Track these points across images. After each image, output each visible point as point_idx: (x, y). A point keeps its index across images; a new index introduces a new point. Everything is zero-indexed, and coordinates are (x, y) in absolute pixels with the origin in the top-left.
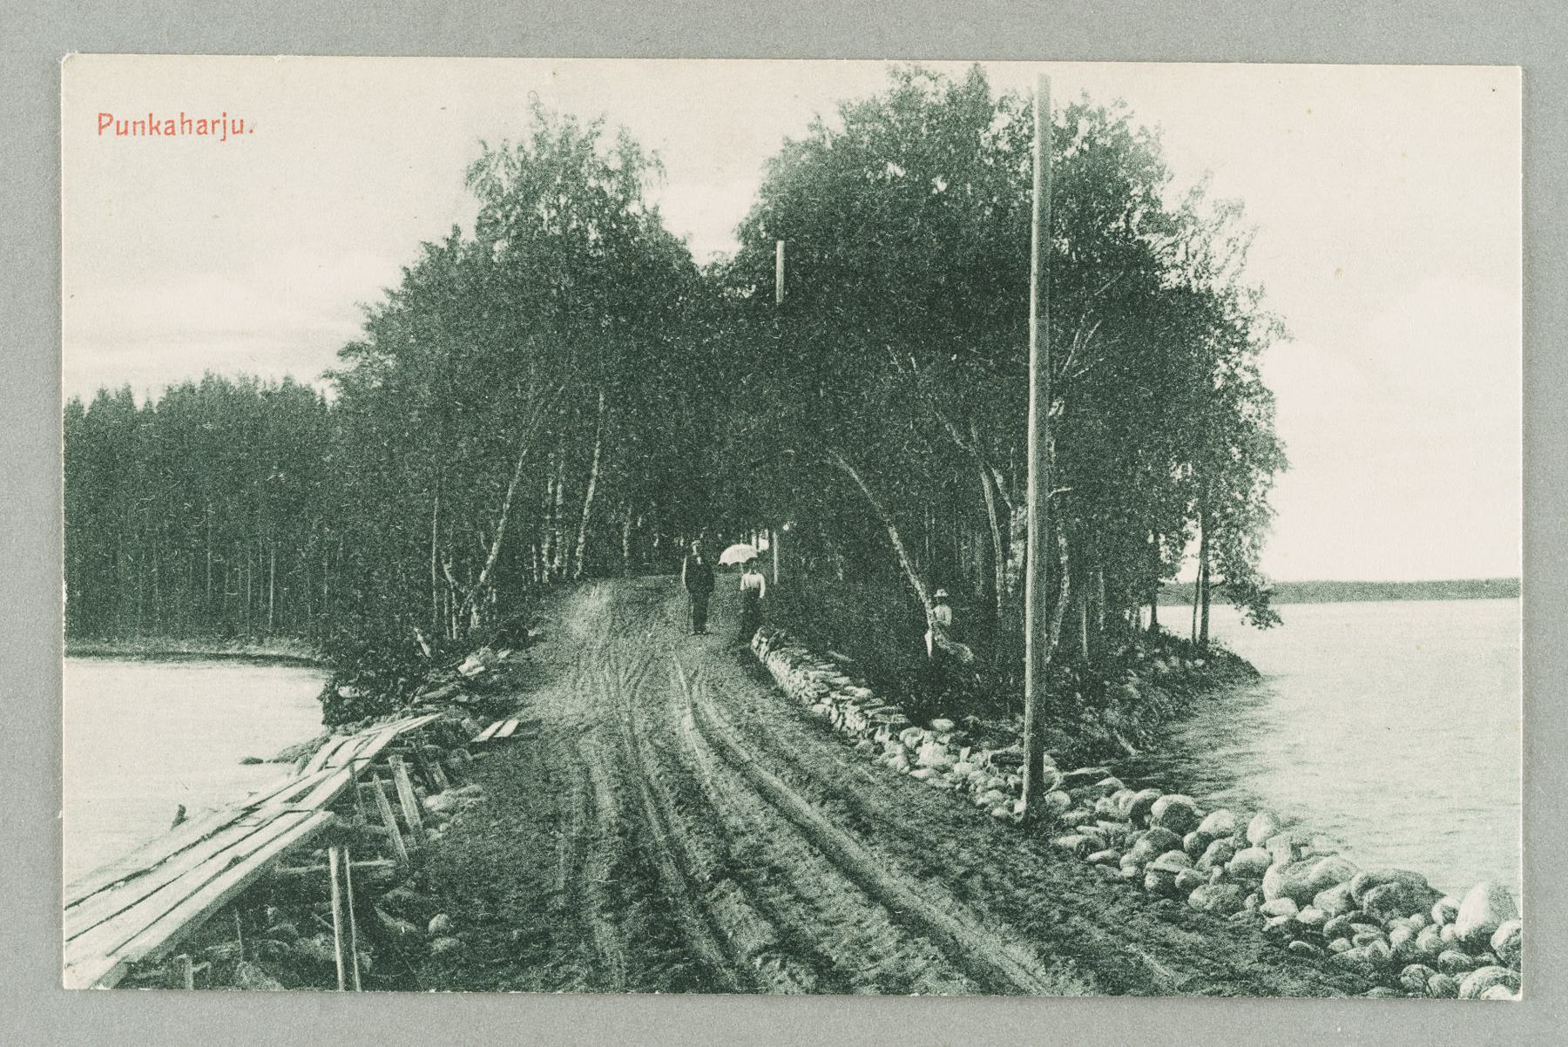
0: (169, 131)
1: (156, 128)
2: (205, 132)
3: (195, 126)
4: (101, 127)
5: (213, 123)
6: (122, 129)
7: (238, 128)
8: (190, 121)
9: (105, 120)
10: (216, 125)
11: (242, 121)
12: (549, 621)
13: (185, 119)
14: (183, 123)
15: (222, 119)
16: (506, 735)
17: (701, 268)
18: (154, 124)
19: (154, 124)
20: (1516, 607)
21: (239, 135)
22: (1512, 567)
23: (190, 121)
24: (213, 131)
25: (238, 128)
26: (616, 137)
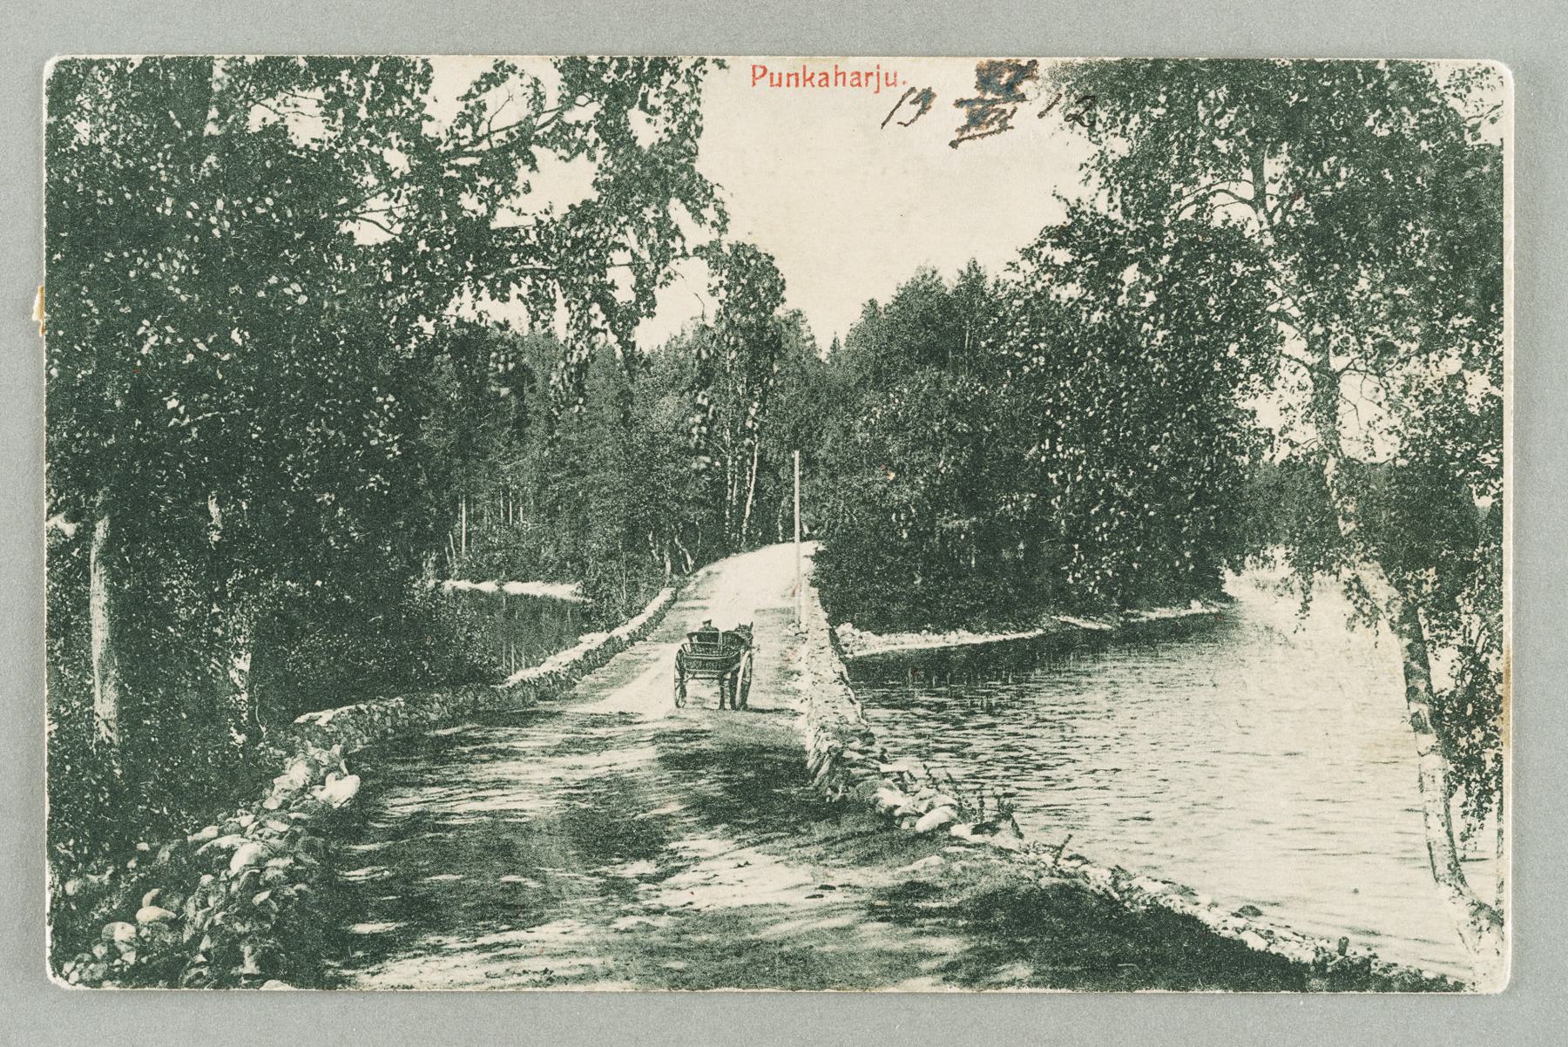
0: (824, 83)
3: (849, 78)
6: (776, 81)
13: (839, 71)
14: (837, 75)
25: (891, 80)
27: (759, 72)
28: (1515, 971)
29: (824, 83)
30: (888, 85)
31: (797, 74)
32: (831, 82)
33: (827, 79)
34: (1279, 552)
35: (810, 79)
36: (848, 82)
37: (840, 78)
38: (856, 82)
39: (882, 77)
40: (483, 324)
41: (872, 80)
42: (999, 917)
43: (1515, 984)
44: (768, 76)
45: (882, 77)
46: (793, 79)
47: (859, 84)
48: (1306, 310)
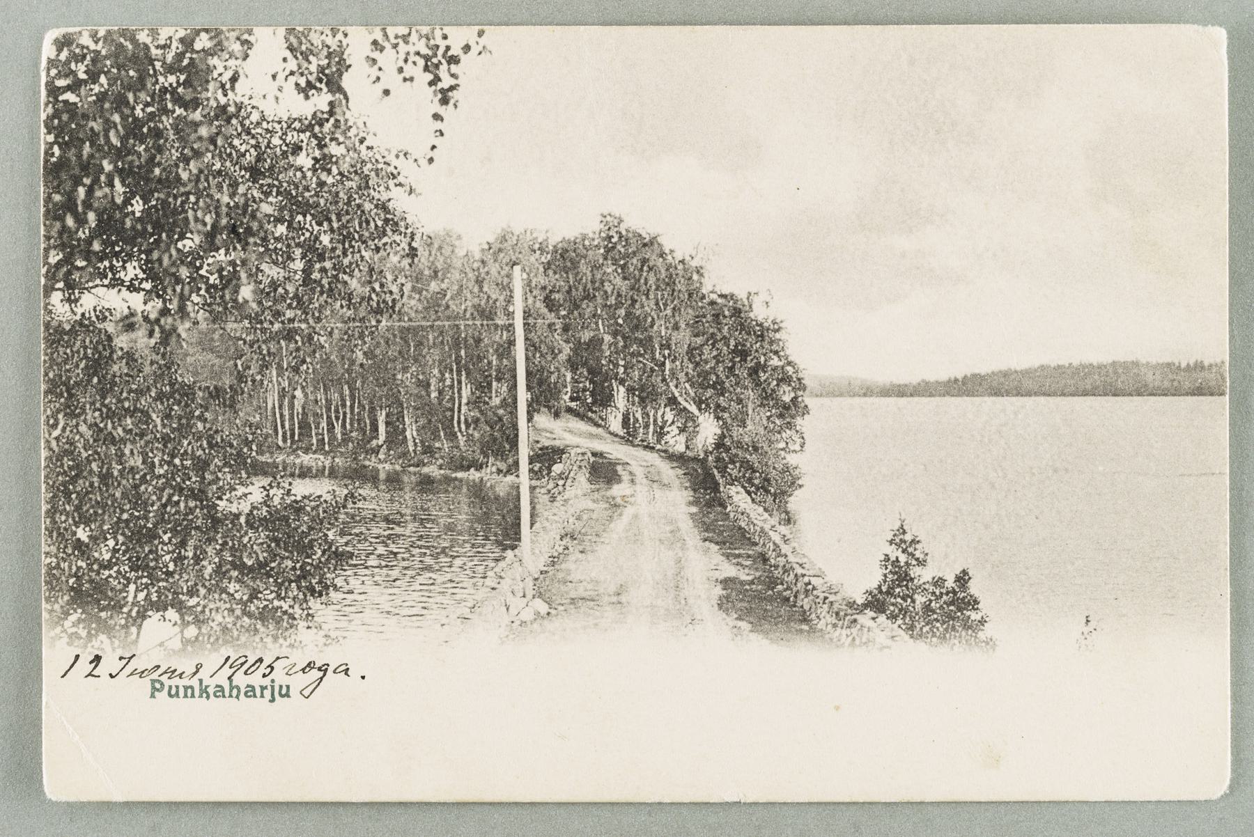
3: (243, 691)
11: (288, 687)
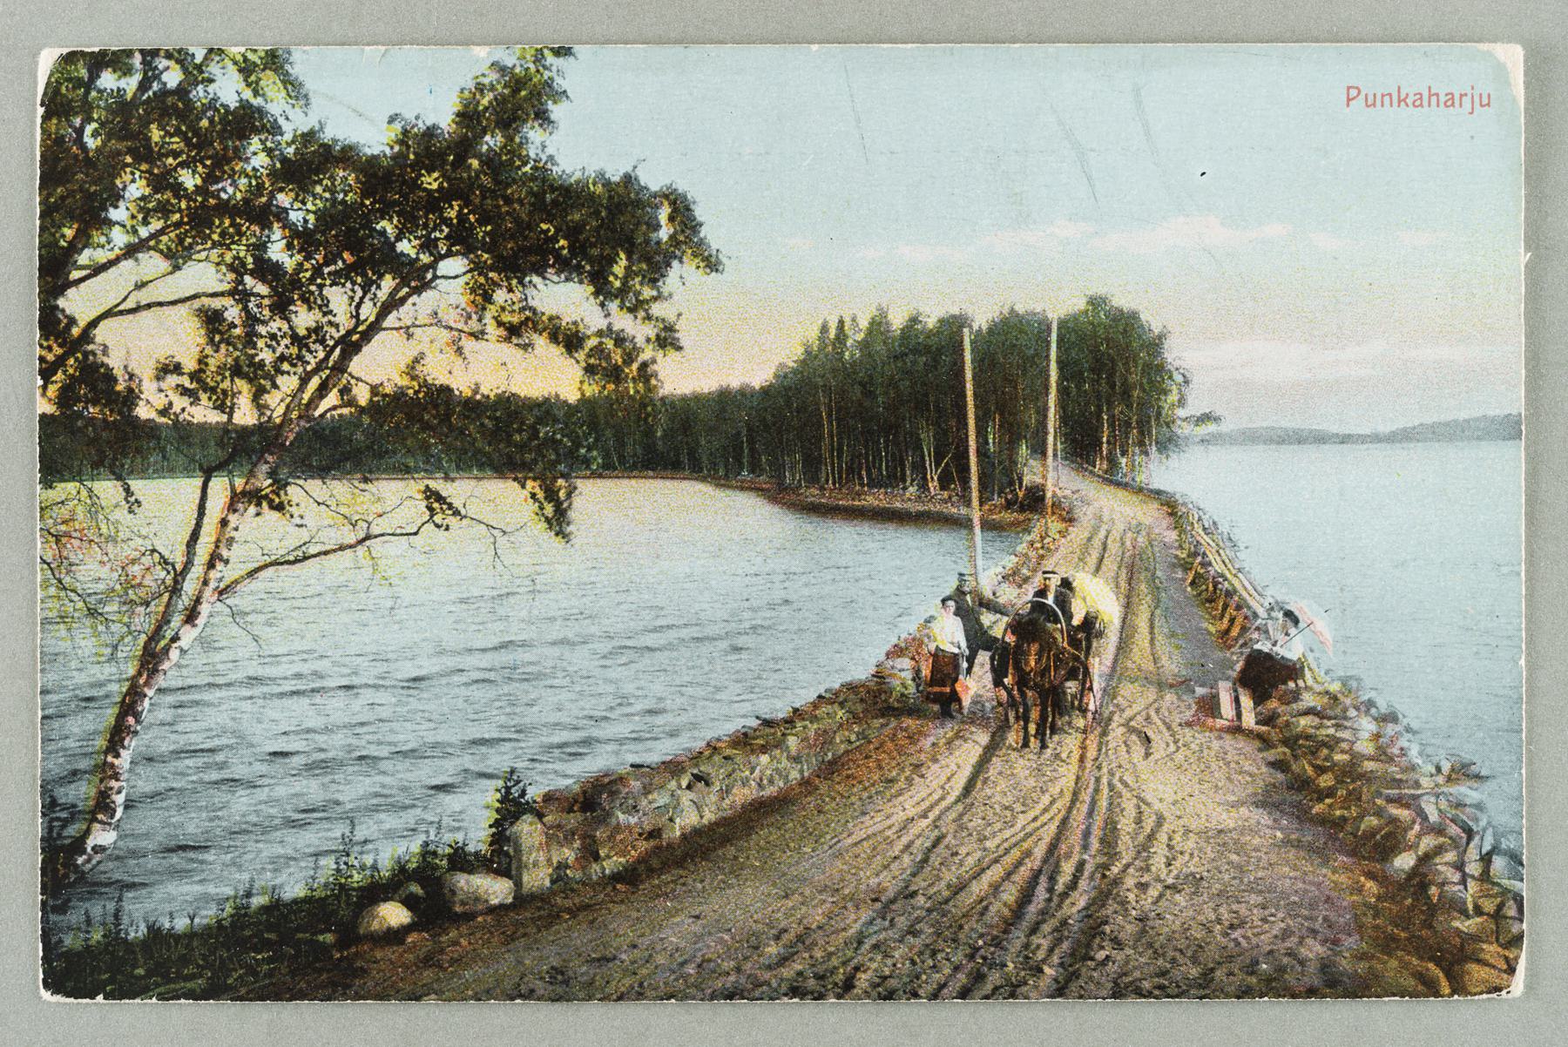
0: (1449, 103)
1: (1404, 100)
2: (1421, 105)
3: (1443, 98)
4: (1349, 100)
5: (1461, 96)
7: (1485, 101)
8: (1437, 95)
9: (1353, 93)
10: (1464, 98)
12: (1425, 859)
13: (1433, 92)
14: (1430, 96)
15: (1469, 92)
16: (1489, 848)
17: (1194, 407)
18: (1402, 97)
19: (1402, 97)
20: (1509, 461)
21: (1371, 109)
22: (1515, 402)
23: (1437, 95)
24: (1461, 105)
25: (1485, 101)
26: (311, 95)
27: (1353, 93)
28: (36, 64)
29: (1449, 103)
30: (1481, 105)
31: (1390, 95)
32: (1378, 103)
33: (1421, 99)
34: (118, 182)
35: (1404, 100)
36: (1442, 104)
37: (1434, 99)
38: (1418, 103)
39: (1477, 100)
40: (144, 167)
41: (1467, 101)
42: (588, 841)
43: (35, 55)
44: (1362, 96)
45: (1477, 100)
46: (1387, 99)
47: (1421, 105)
48: (388, 214)
